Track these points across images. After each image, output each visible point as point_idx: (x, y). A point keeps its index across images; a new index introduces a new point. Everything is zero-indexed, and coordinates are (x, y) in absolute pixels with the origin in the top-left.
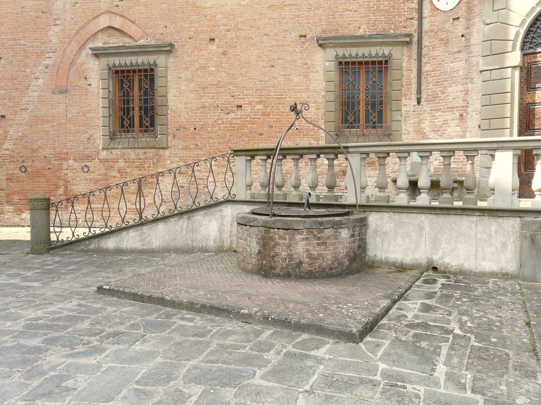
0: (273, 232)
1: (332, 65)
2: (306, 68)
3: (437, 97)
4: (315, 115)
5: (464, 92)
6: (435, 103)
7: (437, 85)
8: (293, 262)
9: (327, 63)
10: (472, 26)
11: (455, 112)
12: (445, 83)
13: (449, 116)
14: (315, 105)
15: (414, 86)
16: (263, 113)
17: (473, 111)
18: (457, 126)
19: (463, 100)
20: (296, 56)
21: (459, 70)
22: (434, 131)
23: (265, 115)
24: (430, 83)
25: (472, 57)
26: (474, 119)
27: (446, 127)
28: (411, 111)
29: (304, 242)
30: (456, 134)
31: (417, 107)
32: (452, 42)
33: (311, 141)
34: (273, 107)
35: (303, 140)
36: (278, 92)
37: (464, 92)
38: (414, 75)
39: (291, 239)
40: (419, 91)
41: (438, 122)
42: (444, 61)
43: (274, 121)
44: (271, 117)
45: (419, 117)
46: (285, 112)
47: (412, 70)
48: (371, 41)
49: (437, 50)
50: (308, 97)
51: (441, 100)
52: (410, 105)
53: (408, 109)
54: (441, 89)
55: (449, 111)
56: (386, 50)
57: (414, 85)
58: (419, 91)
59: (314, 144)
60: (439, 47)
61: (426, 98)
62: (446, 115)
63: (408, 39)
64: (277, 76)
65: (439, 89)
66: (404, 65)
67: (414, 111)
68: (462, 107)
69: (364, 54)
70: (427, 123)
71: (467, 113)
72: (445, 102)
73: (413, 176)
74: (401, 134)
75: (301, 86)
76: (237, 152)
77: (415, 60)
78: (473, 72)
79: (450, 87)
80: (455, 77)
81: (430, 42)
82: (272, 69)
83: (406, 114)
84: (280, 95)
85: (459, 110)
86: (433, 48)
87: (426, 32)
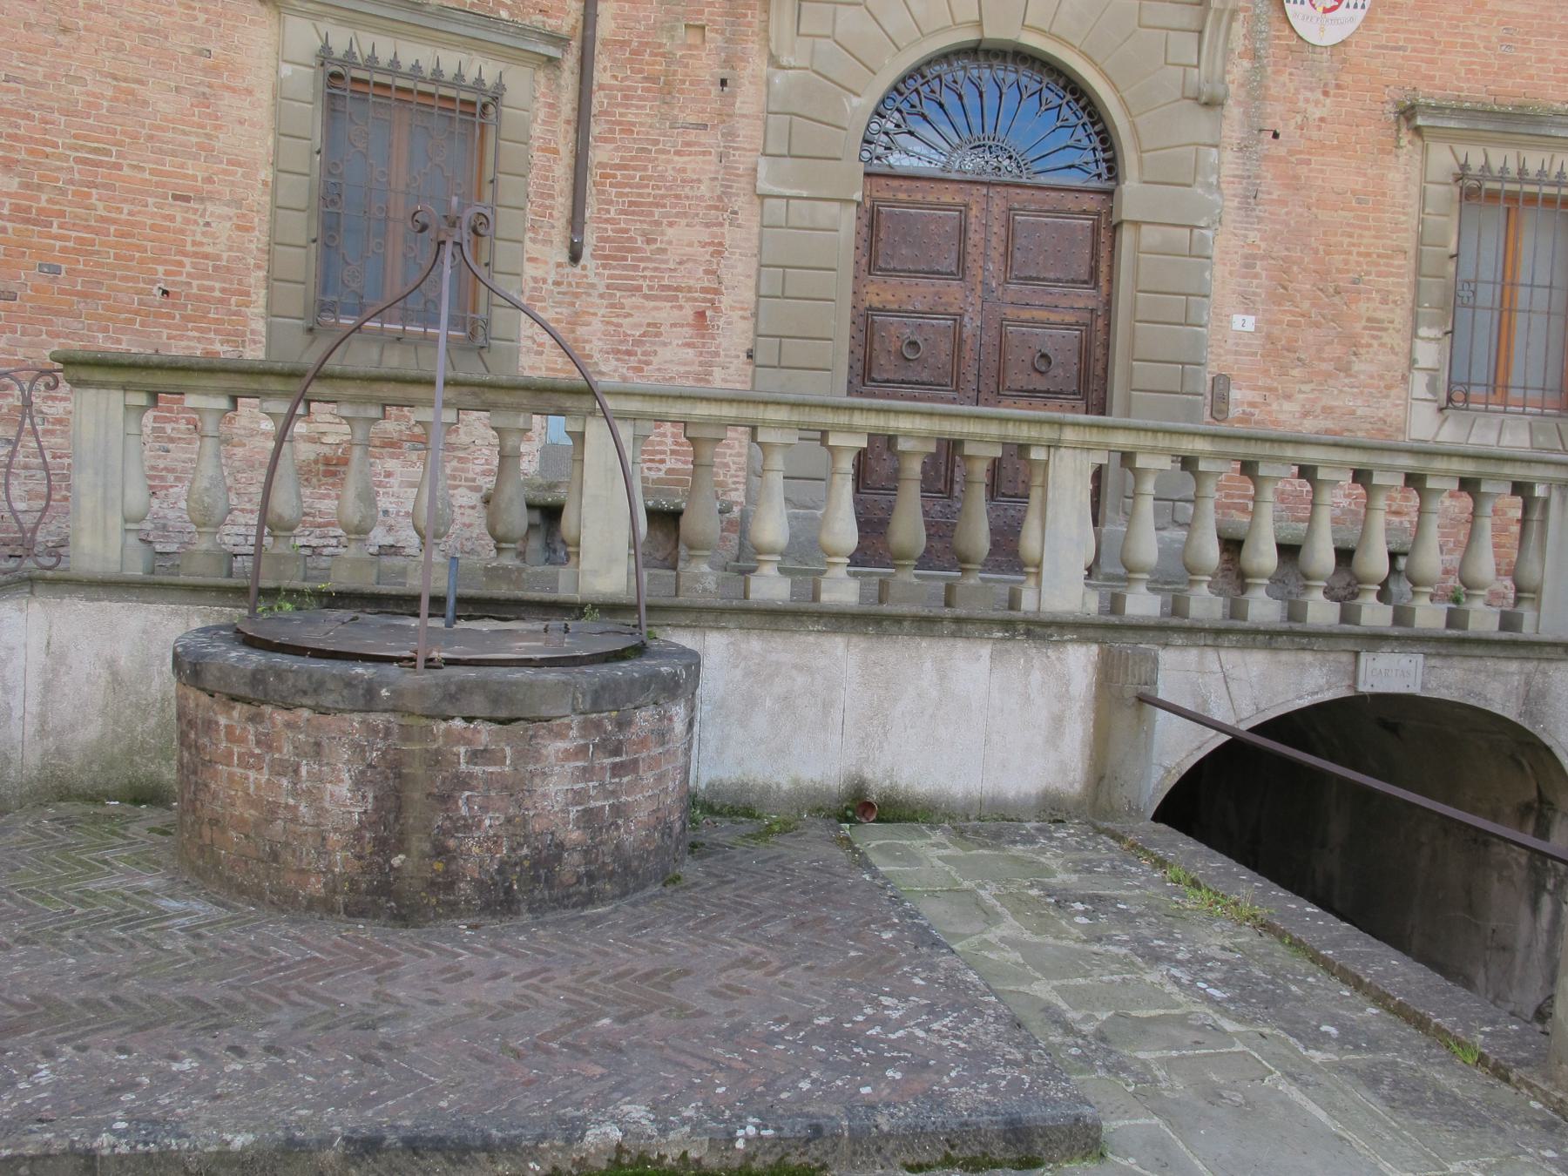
0: (448, 733)
1: (304, 80)
2: (206, 70)
3: (631, 250)
4: (230, 249)
5: (711, 249)
6: (625, 268)
7: (633, 213)
8: (525, 851)
9: (287, 70)
10: (742, 60)
11: (682, 302)
12: (657, 211)
13: (664, 313)
14: (232, 211)
15: (561, 204)
16: (17, 208)
17: (732, 308)
18: (688, 345)
19: (707, 272)
20: (170, 14)
21: (699, 181)
22: (618, 352)
23: (27, 221)
24: (611, 202)
25: (735, 149)
26: (733, 334)
27: (654, 344)
28: (550, 281)
29: (571, 765)
30: (682, 369)
31: (568, 270)
32: (681, 91)
33: (212, 342)
34: (63, 192)
35: (181, 337)
36: (85, 138)
37: (711, 249)
38: (561, 170)
39: (522, 756)
40: (576, 221)
41: (632, 326)
42: (656, 142)
43: (63, 250)
44: (55, 230)
45: (573, 304)
46: (115, 221)
47: (556, 151)
48: (442, 26)
49: (638, 107)
50: (209, 180)
51: (642, 260)
52: (546, 263)
53: (540, 273)
54: (645, 226)
55: (667, 299)
56: (482, 68)
57: (561, 200)
58: (576, 221)
59: (223, 351)
60: (641, 98)
61: (596, 248)
62: (657, 308)
63: (552, 51)
64: (84, 73)
65: (638, 226)
66: (537, 130)
67: (557, 283)
68: (704, 290)
69: (416, 67)
70: (597, 324)
71: (717, 310)
72: (656, 269)
73: (552, 487)
74: (518, 350)
75: (184, 133)
76: (85, 368)
77: (568, 122)
78: (738, 195)
79: (671, 224)
80: (687, 197)
81: (615, 77)
82: (62, 39)
83: (535, 289)
84: (95, 151)
85: (695, 300)
86: (626, 97)
87: (605, 43)
